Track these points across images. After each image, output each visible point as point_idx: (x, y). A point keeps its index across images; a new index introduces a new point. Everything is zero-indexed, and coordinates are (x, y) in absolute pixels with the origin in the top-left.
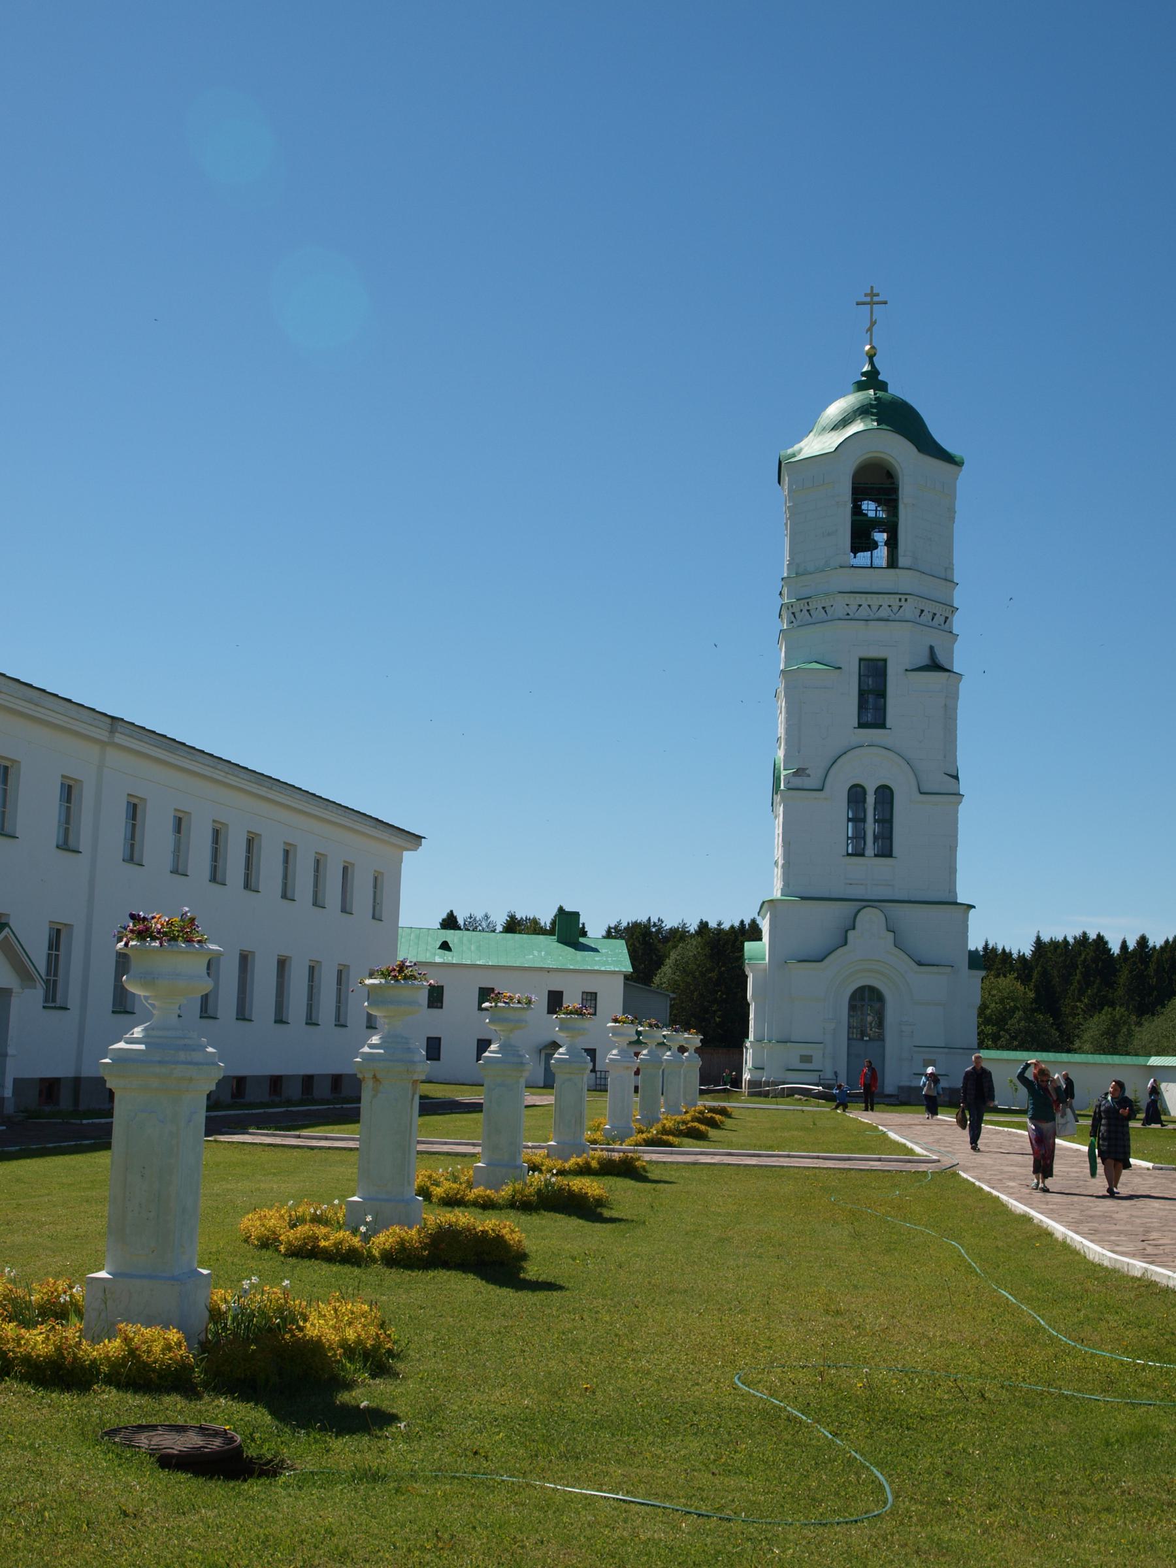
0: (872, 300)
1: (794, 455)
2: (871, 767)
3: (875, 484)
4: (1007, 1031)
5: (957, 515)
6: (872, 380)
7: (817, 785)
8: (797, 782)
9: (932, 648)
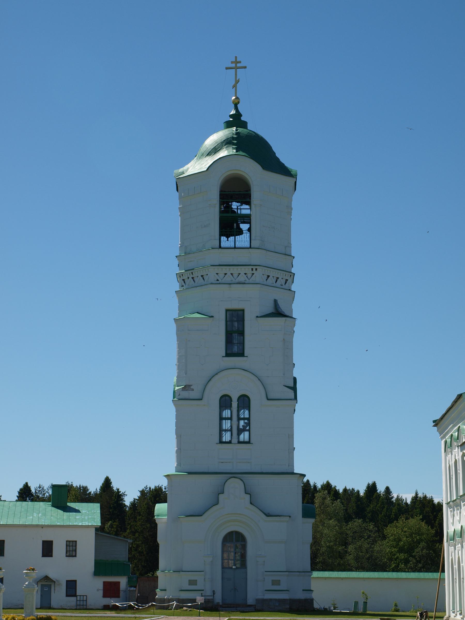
0: (236, 65)
1: (183, 173)
2: (235, 383)
3: (234, 191)
4: (414, 557)
5: (293, 211)
6: (236, 120)
7: (198, 396)
8: (185, 394)
9: (275, 301)
